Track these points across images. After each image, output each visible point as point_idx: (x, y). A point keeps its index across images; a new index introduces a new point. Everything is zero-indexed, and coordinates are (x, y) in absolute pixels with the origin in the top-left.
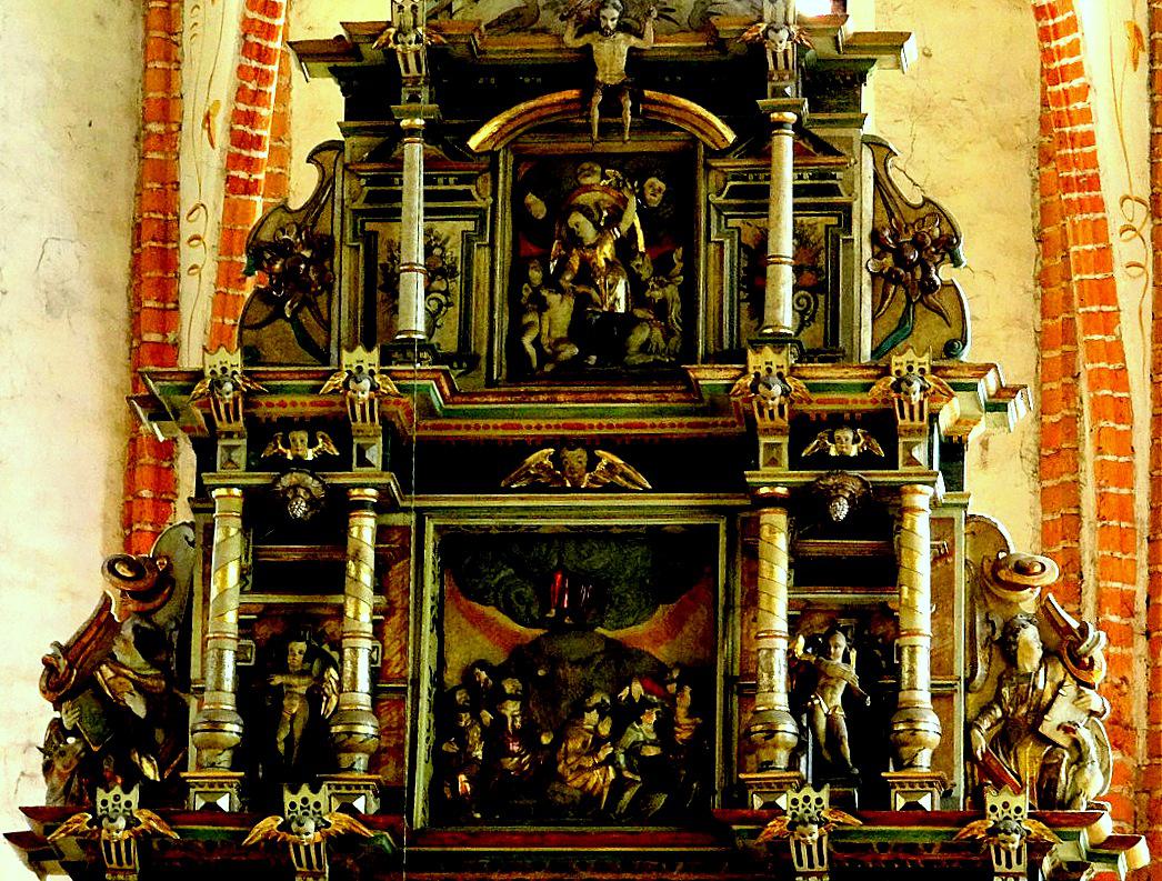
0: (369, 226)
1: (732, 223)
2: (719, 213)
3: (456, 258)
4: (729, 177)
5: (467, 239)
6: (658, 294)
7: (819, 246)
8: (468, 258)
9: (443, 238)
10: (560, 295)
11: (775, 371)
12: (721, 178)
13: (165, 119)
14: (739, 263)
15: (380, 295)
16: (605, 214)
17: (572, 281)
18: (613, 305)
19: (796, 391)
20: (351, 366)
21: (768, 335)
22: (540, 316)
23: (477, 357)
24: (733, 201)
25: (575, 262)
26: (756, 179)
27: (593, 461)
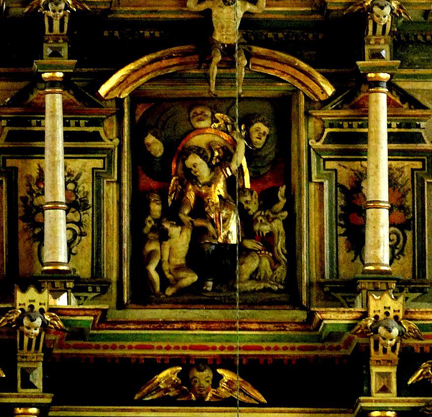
0: (10, 163)
1: (330, 165)
2: (318, 155)
3: (87, 193)
4: (326, 124)
5: (97, 175)
6: (266, 229)
7: (405, 187)
8: (98, 195)
9: (75, 175)
10: (179, 228)
11: (392, 314)
12: (319, 124)
13: (234, 323)
14: (336, 203)
15: (21, 225)
16: (217, 154)
17: (189, 215)
18: (226, 237)
19: (409, 331)
20: (24, 304)
21: (370, 272)
22: (161, 244)
23: (108, 283)
24: (330, 146)
25: (191, 197)
26: (350, 126)
27: (217, 378)
